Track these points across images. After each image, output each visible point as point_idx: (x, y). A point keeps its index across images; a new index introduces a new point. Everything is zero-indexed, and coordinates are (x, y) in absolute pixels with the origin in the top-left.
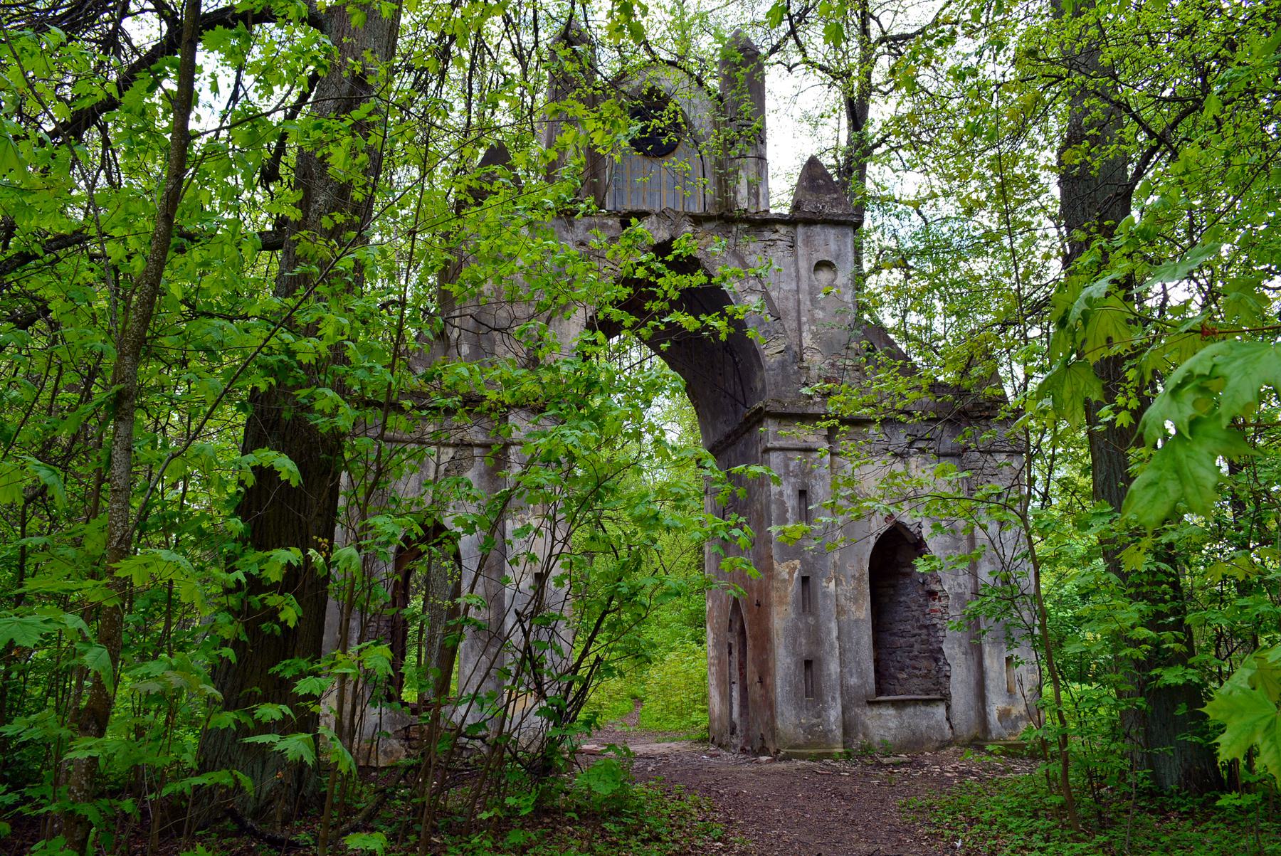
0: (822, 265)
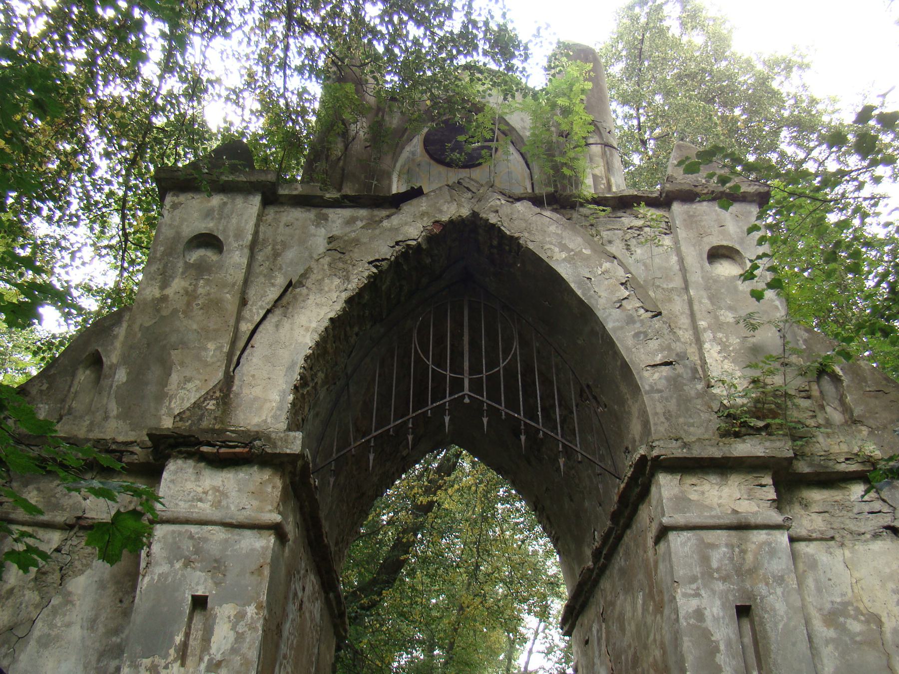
0: (716, 254)
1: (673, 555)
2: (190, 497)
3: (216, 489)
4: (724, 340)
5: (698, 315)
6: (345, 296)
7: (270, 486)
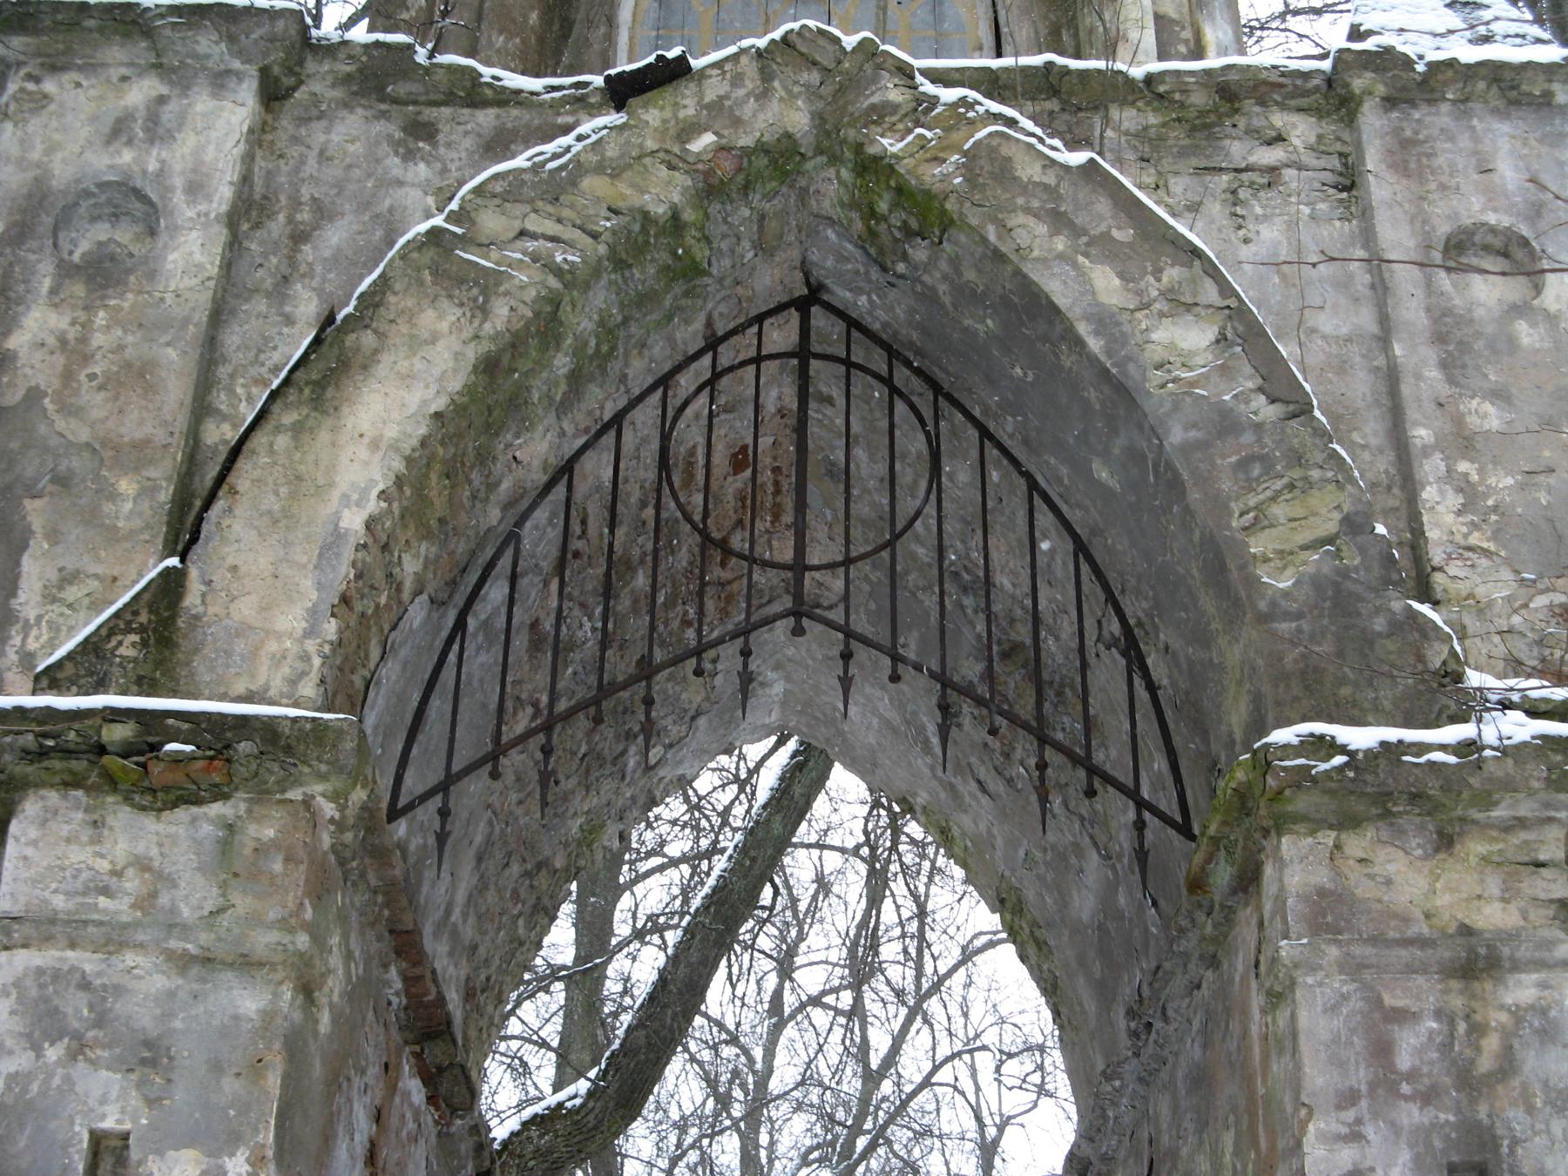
1: (1302, 1039)
2: (79, 885)
3: (143, 865)
4: (1475, 477)
5: (1412, 413)
6: (471, 353)
7: (280, 858)
